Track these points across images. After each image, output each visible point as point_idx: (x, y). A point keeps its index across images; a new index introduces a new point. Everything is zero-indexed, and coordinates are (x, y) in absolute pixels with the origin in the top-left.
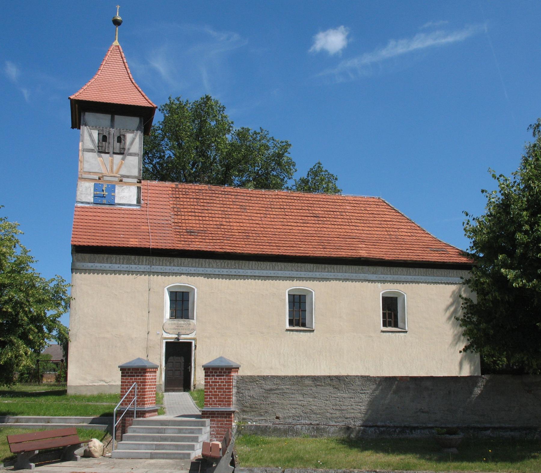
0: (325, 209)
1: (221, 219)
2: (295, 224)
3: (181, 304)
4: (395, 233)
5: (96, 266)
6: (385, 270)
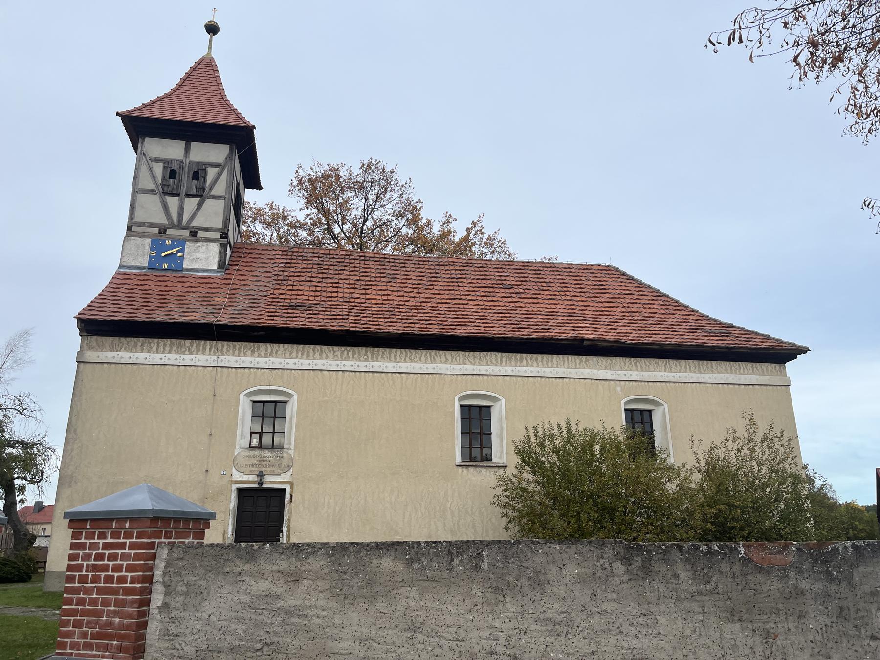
0: (523, 279)
1: (352, 291)
2: (474, 298)
3: (269, 412)
4: (639, 310)
5: (122, 358)
6: (628, 364)
